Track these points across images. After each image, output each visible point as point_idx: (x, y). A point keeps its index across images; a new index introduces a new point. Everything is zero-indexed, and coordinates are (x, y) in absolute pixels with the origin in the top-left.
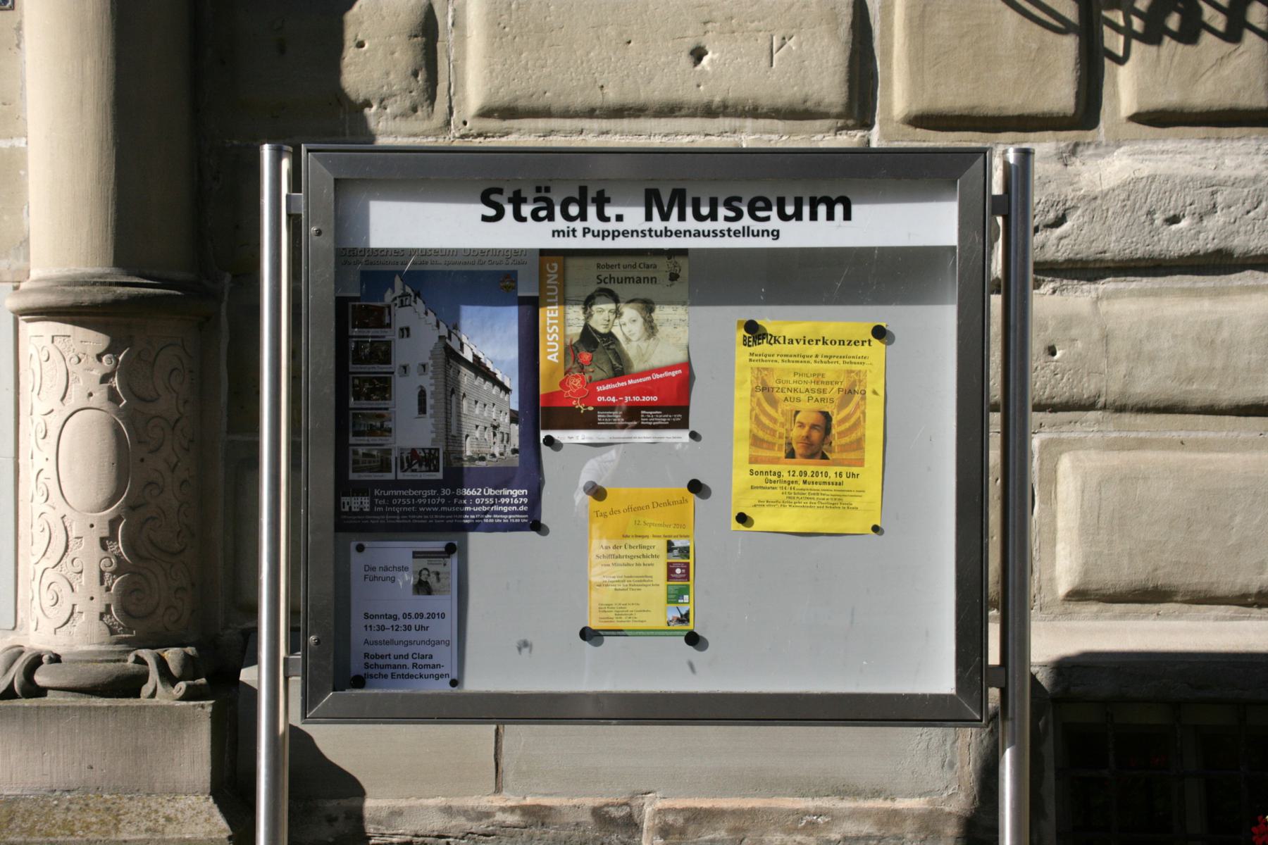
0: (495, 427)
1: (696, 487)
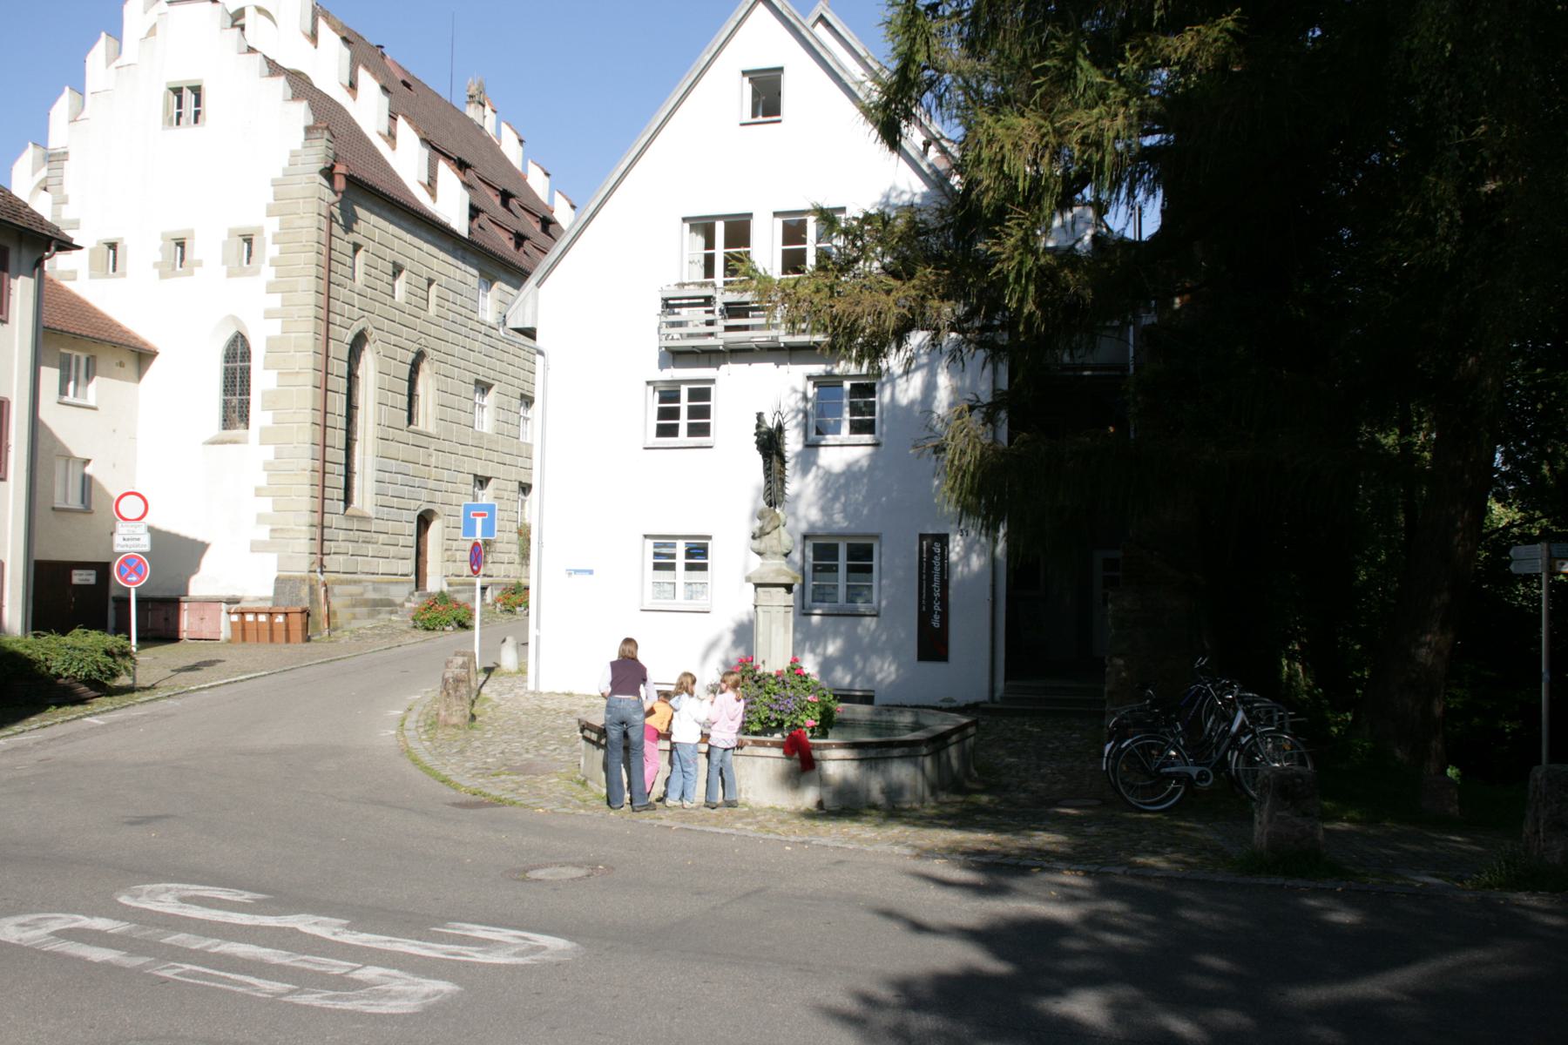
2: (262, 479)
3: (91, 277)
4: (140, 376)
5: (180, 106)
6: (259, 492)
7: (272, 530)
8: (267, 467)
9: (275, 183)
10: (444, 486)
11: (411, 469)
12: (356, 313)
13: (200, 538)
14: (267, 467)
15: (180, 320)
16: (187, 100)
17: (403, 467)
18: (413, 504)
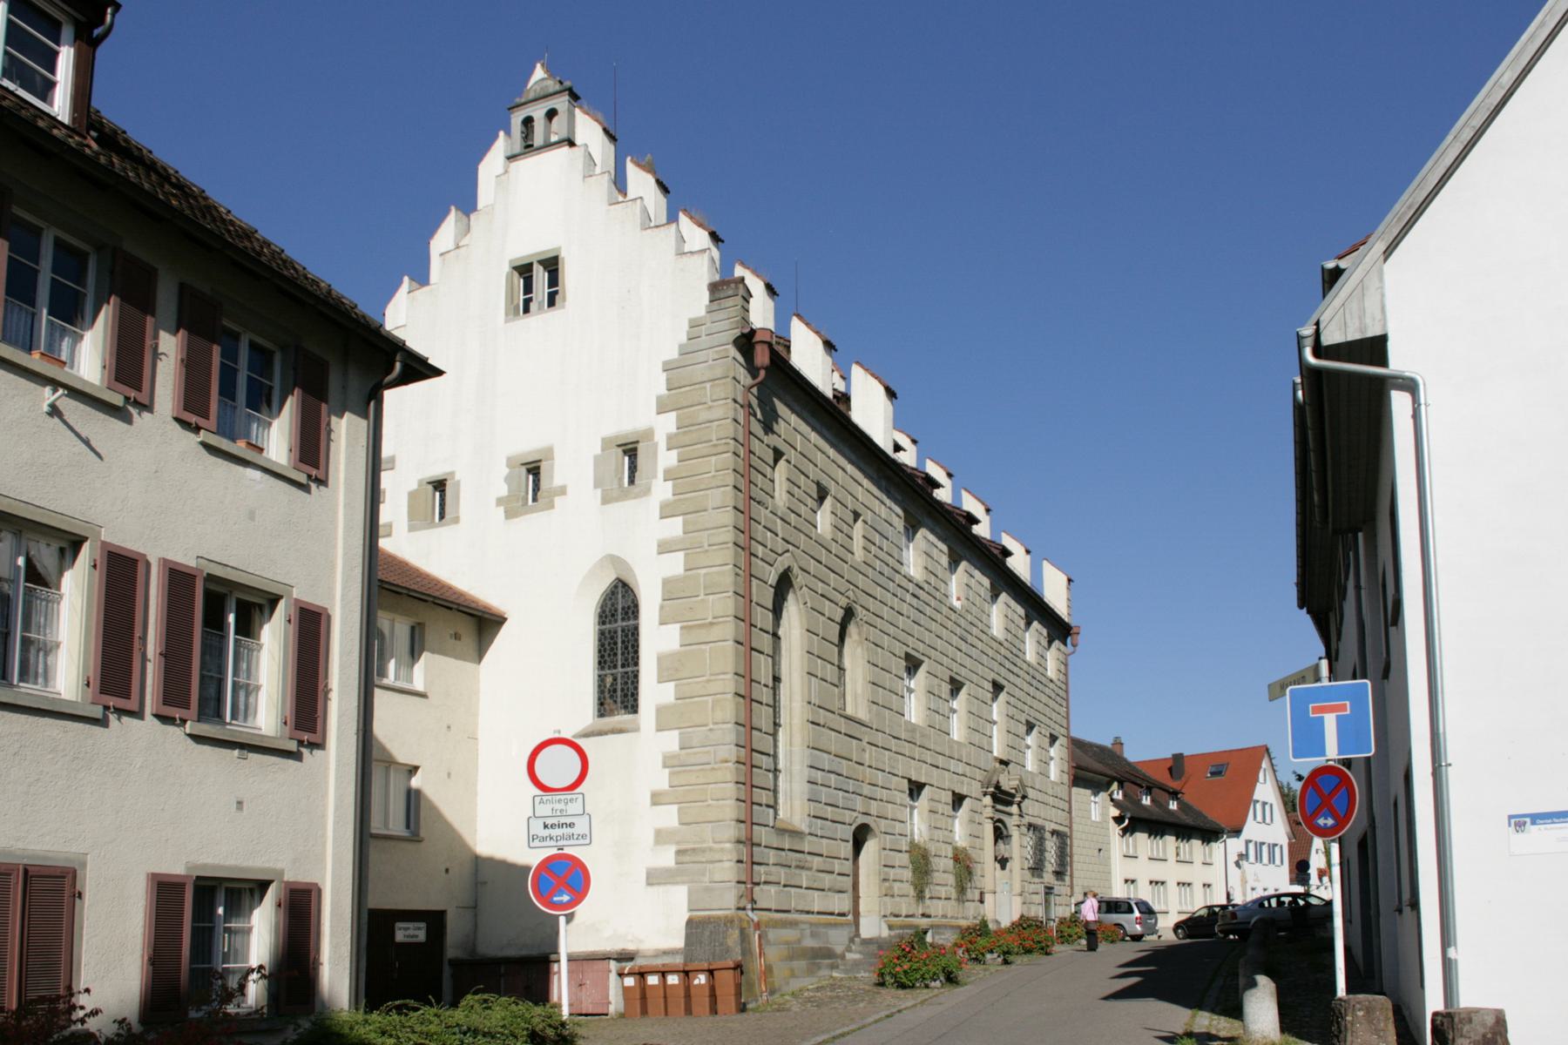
0: (1001, 797)
1: (240, 803)
2: (662, 780)
3: (412, 529)
4: (480, 654)
6: (657, 799)
7: (678, 852)
8: (669, 762)
9: (668, 367)
10: (879, 793)
11: (844, 767)
12: (780, 546)
14: (669, 762)
16: (539, 280)
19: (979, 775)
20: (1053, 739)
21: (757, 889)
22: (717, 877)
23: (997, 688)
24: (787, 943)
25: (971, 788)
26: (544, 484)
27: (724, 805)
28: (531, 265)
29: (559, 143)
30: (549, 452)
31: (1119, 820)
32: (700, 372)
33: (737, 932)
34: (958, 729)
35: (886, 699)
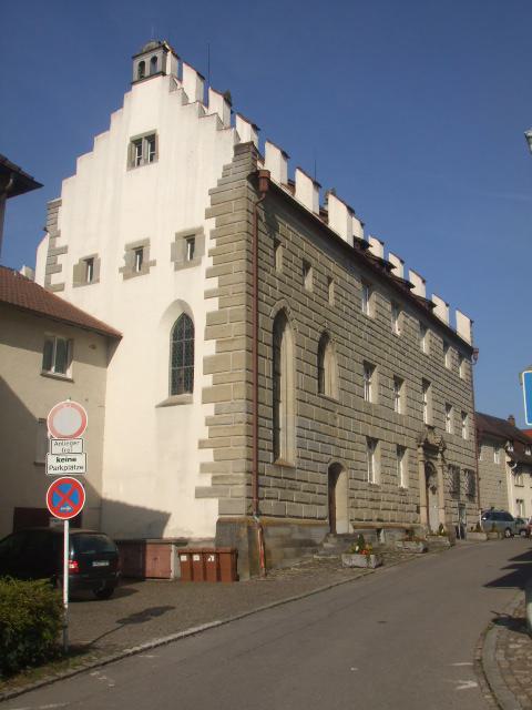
0: (430, 450)
2: (204, 433)
3: (75, 286)
5: (140, 154)
6: (202, 445)
7: (214, 478)
8: (209, 422)
9: (212, 193)
10: (347, 444)
13: (162, 508)
15: (137, 312)
16: (145, 147)
17: (317, 426)
18: (325, 458)
19: (415, 434)
20: (464, 415)
21: (261, 502)
22: (236, 494)
23: (426, 384)
24: (282, 536)
25: (410, 442)
26: (144, 259)
27: (240, 451)
28: (141, 140)
29: (157, 74)
30: (147, 242)
31: (511, 464)
32: (229, 195)
33: (246, 529)
34: (400, 407)
35: (351, 388)
